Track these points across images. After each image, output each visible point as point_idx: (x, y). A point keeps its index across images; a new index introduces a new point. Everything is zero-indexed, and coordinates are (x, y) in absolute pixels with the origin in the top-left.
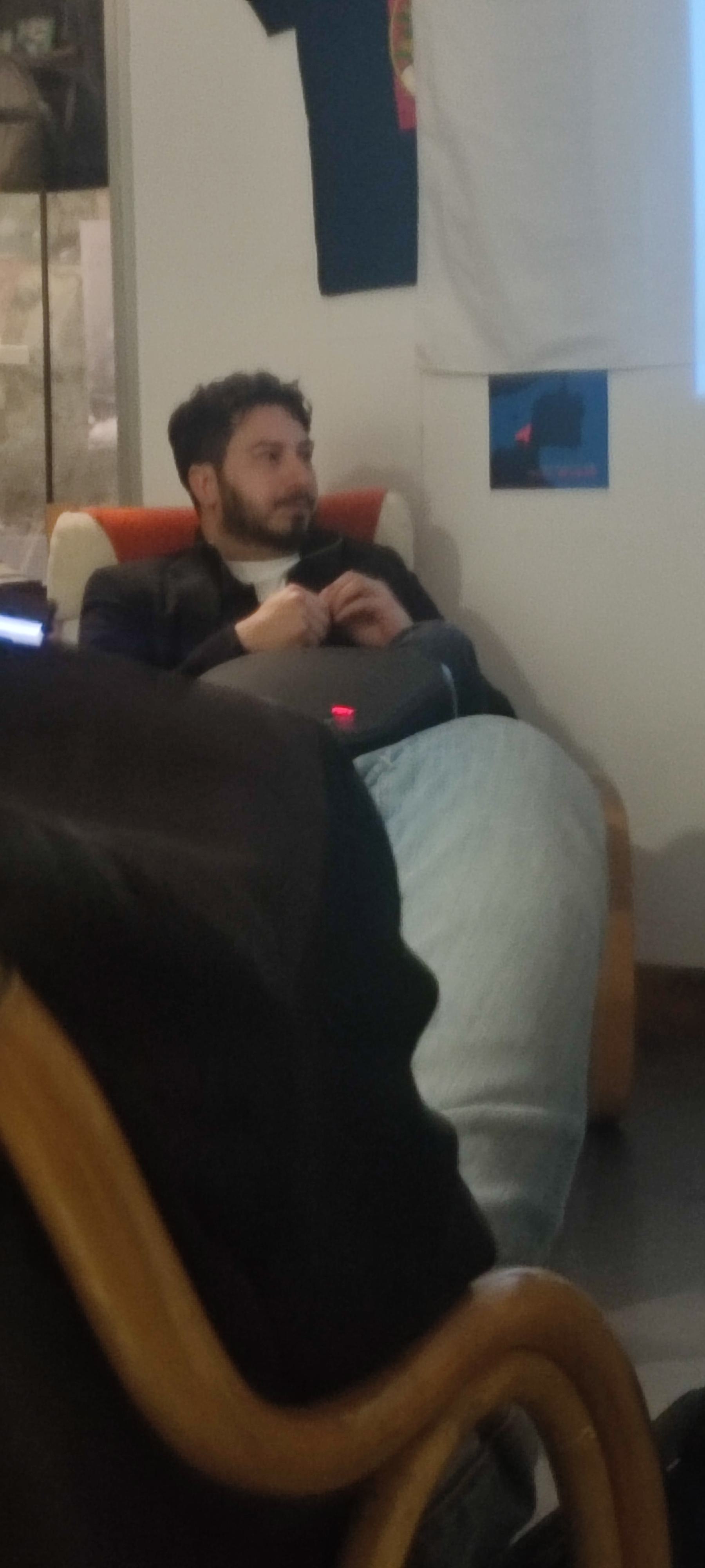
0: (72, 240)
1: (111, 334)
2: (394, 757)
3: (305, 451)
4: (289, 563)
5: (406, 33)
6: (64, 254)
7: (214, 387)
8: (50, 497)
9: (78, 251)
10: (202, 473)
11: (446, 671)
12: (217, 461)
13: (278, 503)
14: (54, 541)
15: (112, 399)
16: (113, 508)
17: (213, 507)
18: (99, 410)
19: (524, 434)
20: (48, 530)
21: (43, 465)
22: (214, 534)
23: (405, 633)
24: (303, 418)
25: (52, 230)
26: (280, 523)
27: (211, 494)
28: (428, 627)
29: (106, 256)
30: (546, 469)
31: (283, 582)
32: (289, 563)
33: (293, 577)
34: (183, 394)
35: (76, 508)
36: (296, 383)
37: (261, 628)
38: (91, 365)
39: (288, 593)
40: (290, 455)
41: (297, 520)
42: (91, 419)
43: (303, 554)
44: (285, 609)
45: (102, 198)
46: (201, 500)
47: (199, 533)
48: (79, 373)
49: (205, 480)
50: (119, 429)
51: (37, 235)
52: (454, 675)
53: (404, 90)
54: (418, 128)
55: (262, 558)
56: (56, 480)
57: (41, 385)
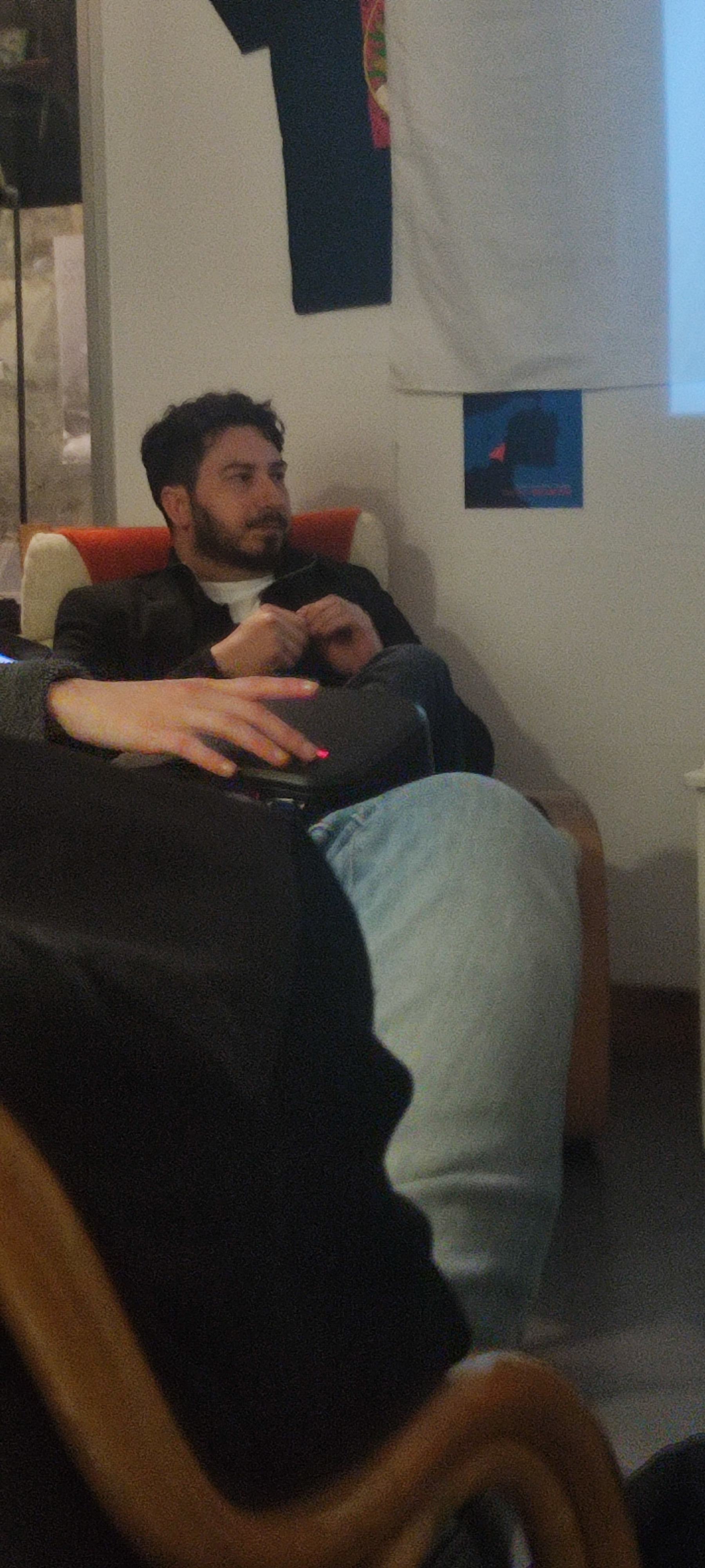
0: (44, 249)
1: (84, 350)
2: (367, 814)
3: (277, 471)
4: (262, 584)
5: (380, 50)
6: (38, 263)
7: (187, 407)
8: (24, 519)
9: (53, 258)
10: (175, 493)
11: (421, 711)
12: (190, 484)
13: (250, 525)
14: (27, 559)
15: (85, 414)
16: (85, 526)
17: (186, 528)
18: (72, 425)
19: (498, 453)
20: (22, 542)
21: (17, 472)
22: (187, 554)
23: (378, 657)
24: (276, 439)
25: (25, 239)
26: (252, 543)
27: (183, 515)
28: (402, 650)
29: (80, 289)
30: (520, 487)
31: (258, 603)
32: (262, 584)
33: (266, 597)
34: (156, 414)
35: (50, 529)
36: (267, 404)
37: (235, 651)
38: (64, 381)
39: (262, 614)
40: (262, 476)
41: (269, 541)
42: (65, 434)
43: (276, 577)
44: (259, 630)
45: (76, 210)
46: (174, 520)
47: (172, 550)
48: (53, 384)
49: (178, 501)
50: (92, 444)
51: (11, 245)
52: (429, 713)
53: (378, 108)
54: (392, 147)
55: (236, 579)
56: (29, 488)
57: (15, 392)
